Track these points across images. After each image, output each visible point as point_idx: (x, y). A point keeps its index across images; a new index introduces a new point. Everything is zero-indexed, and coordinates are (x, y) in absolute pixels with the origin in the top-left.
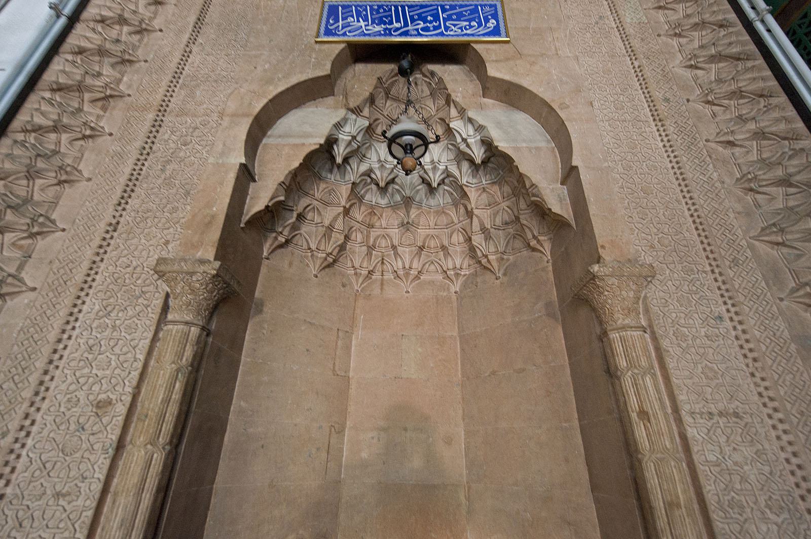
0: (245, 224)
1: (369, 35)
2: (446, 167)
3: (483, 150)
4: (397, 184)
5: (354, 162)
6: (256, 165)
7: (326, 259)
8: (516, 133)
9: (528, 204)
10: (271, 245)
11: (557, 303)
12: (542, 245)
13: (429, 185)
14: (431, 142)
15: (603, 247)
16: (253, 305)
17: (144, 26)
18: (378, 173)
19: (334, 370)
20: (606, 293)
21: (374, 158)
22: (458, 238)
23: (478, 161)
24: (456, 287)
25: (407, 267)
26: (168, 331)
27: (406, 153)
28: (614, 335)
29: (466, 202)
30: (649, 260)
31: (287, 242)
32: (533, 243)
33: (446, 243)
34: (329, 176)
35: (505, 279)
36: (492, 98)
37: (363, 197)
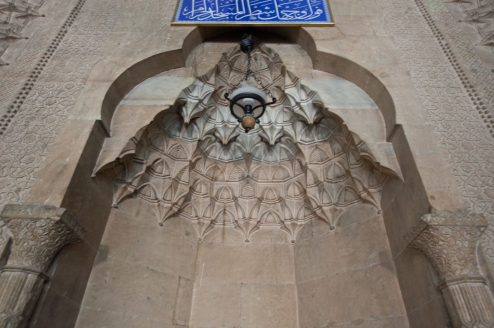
0: (96, 174)
1: (216, 20)
2: (282, 127)
3: (314, 112)
4: (238, 142)
5: (200, 122)
6: (112, 122)
7: (171, 209)
8: (344, 99)
9: (358, 159)
10: (120, 195)
11: (390, 253)
12: (372, 197)
13: (267, 143)
14: (269, 104)
15: (432, 197)
16: (98, 253)
17: (30, 12)
18: (222, 132)
19: (173, 319)
20: (441, 243)
21: (219, 119)
22: (294, 190)
23: (311, 121)
24: (293, 236)
25: (247, 217)
26: (5, 277)
27: (246, 112)
28: (454, 287)
29: (301, 158)
30: (478, 211)
31: (136, 192)
32: (364, 195)
33: (283, 195)
34: (178, 134)
35: (339, 229)
36: (321, 70)
37: (208, 153)
